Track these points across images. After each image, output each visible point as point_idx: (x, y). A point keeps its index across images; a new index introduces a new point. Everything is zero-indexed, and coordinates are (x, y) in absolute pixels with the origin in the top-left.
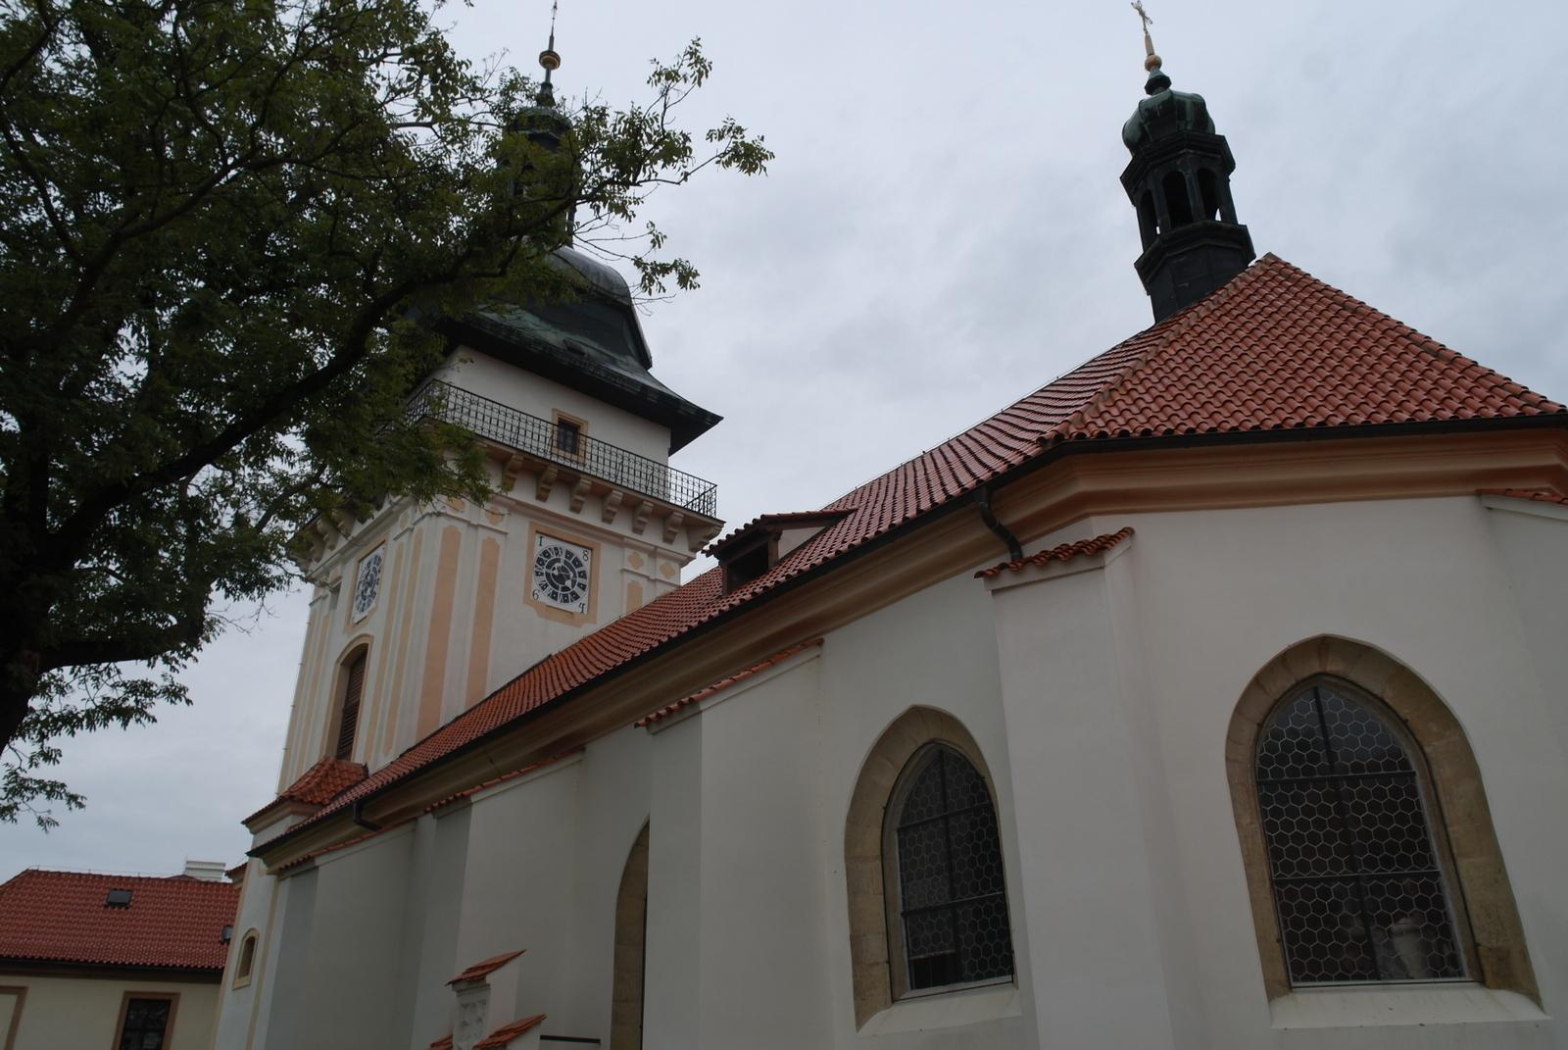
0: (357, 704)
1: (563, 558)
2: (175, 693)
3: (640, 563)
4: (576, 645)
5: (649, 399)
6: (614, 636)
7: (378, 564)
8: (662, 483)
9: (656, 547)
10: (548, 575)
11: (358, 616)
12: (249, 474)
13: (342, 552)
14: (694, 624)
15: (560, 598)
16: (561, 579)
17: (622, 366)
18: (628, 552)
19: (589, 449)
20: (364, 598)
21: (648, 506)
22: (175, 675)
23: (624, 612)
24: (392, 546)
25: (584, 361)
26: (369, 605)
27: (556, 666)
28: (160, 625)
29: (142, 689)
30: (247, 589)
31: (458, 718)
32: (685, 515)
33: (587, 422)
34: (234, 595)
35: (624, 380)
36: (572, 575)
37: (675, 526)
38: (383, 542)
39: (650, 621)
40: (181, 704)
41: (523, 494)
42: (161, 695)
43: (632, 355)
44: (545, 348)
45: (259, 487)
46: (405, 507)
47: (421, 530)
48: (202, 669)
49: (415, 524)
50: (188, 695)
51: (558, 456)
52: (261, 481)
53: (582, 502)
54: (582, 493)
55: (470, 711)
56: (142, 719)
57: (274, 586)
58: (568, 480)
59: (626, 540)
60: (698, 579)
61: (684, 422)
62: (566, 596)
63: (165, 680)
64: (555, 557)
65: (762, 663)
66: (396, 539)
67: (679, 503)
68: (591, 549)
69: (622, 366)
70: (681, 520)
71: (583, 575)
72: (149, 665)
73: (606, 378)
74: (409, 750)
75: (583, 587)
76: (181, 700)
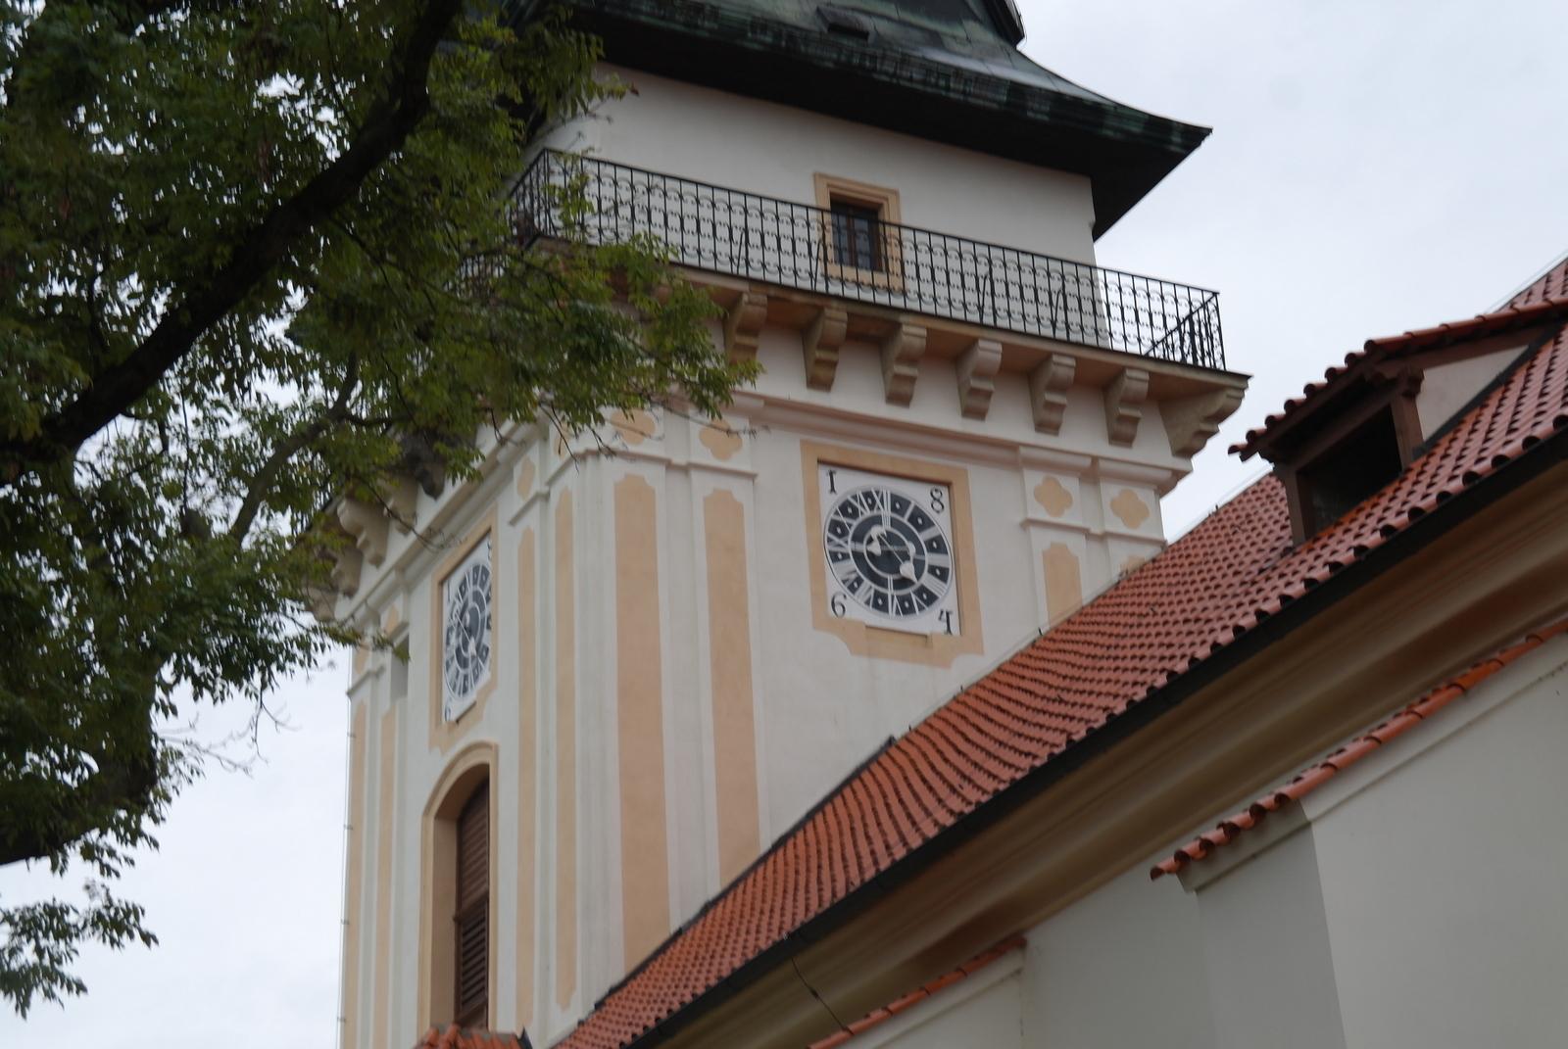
0: (484, 900)
1: (886, 513)
2: (116, 923)
3: (1064, 501)
4: (947, 708)
5: (1030, 114)
6: (1039, 675)
7: (483, 585)
8: (1087, 306)
9: (1095, 459)
10: (858, 556)
11: (456, 706)
12: (196, 422)
13: (402, 567)
14: (1248, 621)
15: (893, 605)
16: (889, 562)
17: (957, 47)
18: (1034, 479)
19: (909, 255)
20: (464, 663)
21: (1063, 366)
22: (111, 882)
23: (1043, 620)
24: (508, 539)
25: (870, 50)
26: (476, 678)
27: (912, 762)
28: (67, 778)
29: (48, 923)
30: (237, 673)
31: (708, 907)
32: (1151, 374)
33: (896, 193)
34: (212, 691)
35: (967, 81)
36: (912, 549)
37: (1133, 401)
38: (488, 532)
39: (1121, 630)
40: (133, 946)
41: (779, 379)
42: (89, 929)
43: (976, 19)
44: (778, 36)
45: (222, 447)
46: (524, 445)
47: (566, 495)
48: (167, 863)
49: (551, 482)
50: (146, 924)
51: (843, 281)
52: (224, 432)
53: (912, 380)
54: (909, 359)
55: (734, 885)
56: (56, 989)
57: (291, 658)
58: (873, 332)
59: (1023, 450)
60: (1217, 517)
61: (1118, 155)
62: (908, 598)
63: (92, 897)
64: (868, 513)
65: (1436, 691)
66: (514, 522)
67: (1133, 348)
68: (948, 485)
69: (957, 47)
70: (1145, 387)
71: (937, 545)
72: (54, 868)
73: (651, 15)
74: (613, 991)
75: (942, 574)
76: (131, 936)
